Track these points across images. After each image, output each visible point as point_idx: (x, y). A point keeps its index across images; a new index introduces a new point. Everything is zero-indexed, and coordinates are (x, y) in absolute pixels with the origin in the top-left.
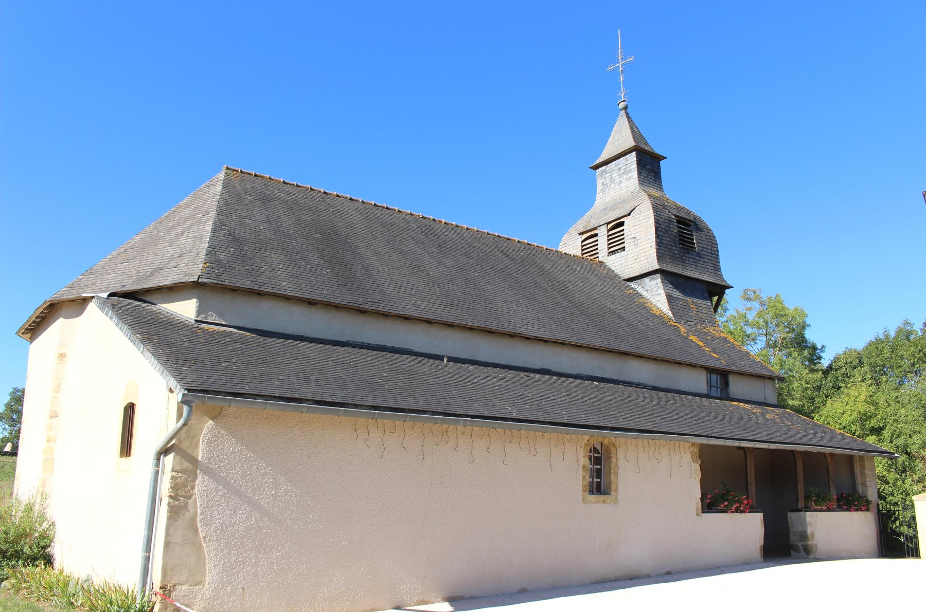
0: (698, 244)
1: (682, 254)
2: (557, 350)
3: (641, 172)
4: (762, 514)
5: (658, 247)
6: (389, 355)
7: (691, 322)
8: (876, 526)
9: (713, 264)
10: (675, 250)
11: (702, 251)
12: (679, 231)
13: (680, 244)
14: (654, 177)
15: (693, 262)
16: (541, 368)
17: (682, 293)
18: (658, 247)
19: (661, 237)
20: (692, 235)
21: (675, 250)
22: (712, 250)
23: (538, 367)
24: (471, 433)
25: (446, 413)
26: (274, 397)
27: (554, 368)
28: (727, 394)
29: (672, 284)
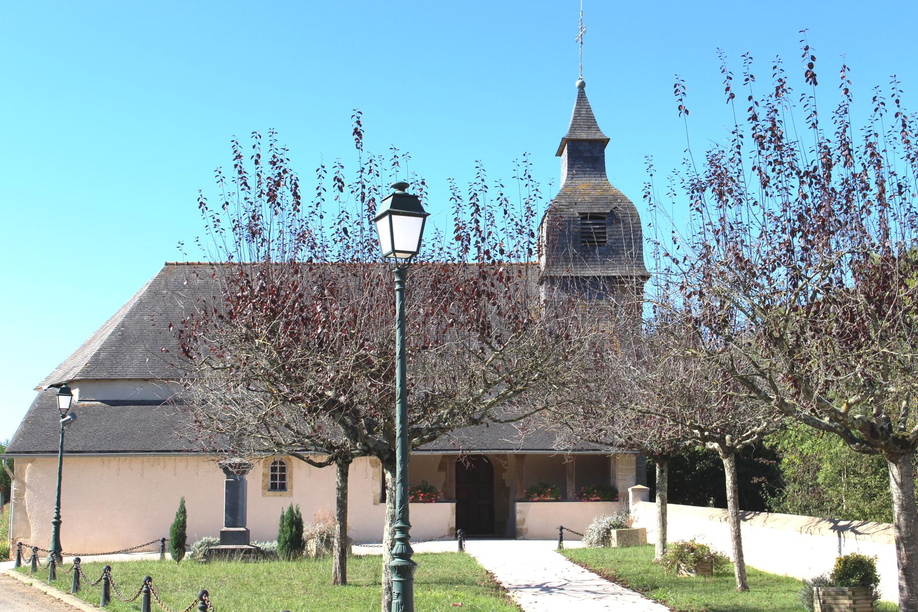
11: (615, 243)
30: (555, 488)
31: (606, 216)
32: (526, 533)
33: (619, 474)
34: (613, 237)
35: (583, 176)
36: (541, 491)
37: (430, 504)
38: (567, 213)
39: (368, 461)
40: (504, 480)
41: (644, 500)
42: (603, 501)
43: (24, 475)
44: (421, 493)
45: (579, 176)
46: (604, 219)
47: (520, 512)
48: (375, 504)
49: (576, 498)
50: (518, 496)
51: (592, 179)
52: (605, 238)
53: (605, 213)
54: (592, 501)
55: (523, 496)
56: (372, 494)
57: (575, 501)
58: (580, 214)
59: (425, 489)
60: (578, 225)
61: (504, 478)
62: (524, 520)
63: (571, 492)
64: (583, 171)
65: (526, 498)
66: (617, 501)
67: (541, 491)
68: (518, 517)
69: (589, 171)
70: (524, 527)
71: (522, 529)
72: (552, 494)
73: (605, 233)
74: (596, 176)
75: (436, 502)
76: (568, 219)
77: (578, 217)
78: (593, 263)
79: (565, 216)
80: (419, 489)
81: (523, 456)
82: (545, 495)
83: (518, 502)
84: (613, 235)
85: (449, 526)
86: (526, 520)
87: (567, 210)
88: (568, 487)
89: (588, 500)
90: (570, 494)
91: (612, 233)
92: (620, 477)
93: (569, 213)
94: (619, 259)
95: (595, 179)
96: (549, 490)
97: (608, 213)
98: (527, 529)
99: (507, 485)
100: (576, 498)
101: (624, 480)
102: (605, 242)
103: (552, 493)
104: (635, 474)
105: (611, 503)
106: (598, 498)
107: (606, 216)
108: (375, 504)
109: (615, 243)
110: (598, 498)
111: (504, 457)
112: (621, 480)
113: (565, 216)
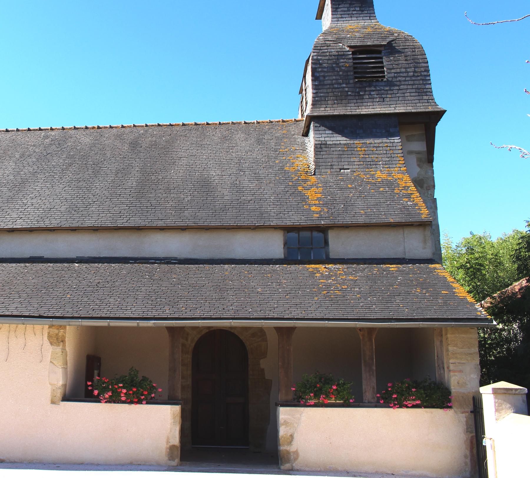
0: (389, 71)
1: (358, 90)
2: (51, 237)
3: (337, 8)
4: (177, 409)
5: (315, 91)
6: (207, 266)
7: (348, 169)
8: (468, 431)
9: (417, 88)
10: (345, 87)
11: (396, 77)
12: (354, 63)
13: (356, 78)
14: (360, 7)
15: (377, 95)
16: (30, 257)
17: (346, 137)
18: (315, 91)
19: (322, 78)
20: (382, 63)
21: (345, 87)
22: (408, 72)
23: (27, 255)
24: (26, 330)
25: (448, 319)
26: (392, 319)
27: (47, 254)
28: (327, 255)
29: (330, 129)
30: (344, 384)
31: (382, 49)
32: (296, 459)
33: (451, 361)
34: (393, 71)
35: (350, 19)
36: (321, 389)
37: (139, 406)
38: (335, 47)
39: (46, 335)
40: (263, 370)
41: (517, 412)
42: (425, 407)
43: (443, 352)
44: (123, 387)
45: (344, 19)
46: (380, 52)
47: (286, 423)
48: (53, 402)
49: (378, 402)
50: (282, 397)
51: (361, 21)
52: (383, 72)
53: (381, 46)
54: (407, 407)
55: (290, 397)
56: (50, 387)
57: (376, 405)
58: (350, 47)
59: (132, 381)
60: (349, 59)
61: (262, 366)
62: (292, 436)
63: (369, 391)
64: (349, 14)
65: (294, 399)
66: (450, 407)
67: (321, 389)
68: (283, 431)
69: (357, 14)
70: (292, 448)
71: (288, 452)
72: (338, 394)
73: (383, 67)
74: (364, 18)
75: (147, 403)
76: (337, 54)
77: (348, 51)
78: (370, 100)
79: (333, 50)
80: (121, 382)
81: (291, 330)
82: (328, 396)
83: (283, 405)
84: (393, 69)
85: (168, 442)
86: (295, 436)
87: (335, 45)
88: (364, 382)
89: (401, 406)
90: (369, 391)
91: (391, 67)
92: (452, 367)
93: (338, 47)
94: (402, 95)
95: (364, 21)
96: (334, 387)
97: (384, 45)
98: (296, 453)
99: (268, 376)
100: (378, 402)
101: (461, 371)
102: (384, 77)
103: (339, 393)
104: (478, 363)
105: (439, 411)
106: (418, 402)
107: (382, 49)
108: (53, 402)
109: (396, 77)
110: (418, 402)
111: (260, 332)
112: (454, 371)
113: (333, 50)
